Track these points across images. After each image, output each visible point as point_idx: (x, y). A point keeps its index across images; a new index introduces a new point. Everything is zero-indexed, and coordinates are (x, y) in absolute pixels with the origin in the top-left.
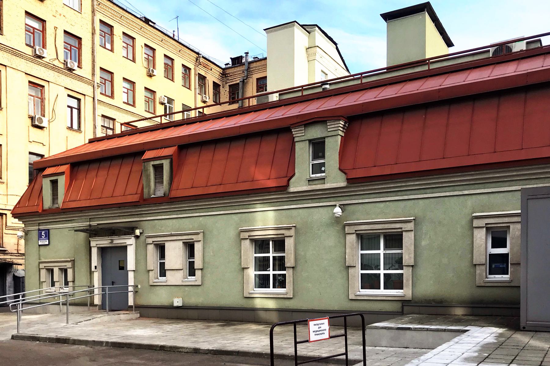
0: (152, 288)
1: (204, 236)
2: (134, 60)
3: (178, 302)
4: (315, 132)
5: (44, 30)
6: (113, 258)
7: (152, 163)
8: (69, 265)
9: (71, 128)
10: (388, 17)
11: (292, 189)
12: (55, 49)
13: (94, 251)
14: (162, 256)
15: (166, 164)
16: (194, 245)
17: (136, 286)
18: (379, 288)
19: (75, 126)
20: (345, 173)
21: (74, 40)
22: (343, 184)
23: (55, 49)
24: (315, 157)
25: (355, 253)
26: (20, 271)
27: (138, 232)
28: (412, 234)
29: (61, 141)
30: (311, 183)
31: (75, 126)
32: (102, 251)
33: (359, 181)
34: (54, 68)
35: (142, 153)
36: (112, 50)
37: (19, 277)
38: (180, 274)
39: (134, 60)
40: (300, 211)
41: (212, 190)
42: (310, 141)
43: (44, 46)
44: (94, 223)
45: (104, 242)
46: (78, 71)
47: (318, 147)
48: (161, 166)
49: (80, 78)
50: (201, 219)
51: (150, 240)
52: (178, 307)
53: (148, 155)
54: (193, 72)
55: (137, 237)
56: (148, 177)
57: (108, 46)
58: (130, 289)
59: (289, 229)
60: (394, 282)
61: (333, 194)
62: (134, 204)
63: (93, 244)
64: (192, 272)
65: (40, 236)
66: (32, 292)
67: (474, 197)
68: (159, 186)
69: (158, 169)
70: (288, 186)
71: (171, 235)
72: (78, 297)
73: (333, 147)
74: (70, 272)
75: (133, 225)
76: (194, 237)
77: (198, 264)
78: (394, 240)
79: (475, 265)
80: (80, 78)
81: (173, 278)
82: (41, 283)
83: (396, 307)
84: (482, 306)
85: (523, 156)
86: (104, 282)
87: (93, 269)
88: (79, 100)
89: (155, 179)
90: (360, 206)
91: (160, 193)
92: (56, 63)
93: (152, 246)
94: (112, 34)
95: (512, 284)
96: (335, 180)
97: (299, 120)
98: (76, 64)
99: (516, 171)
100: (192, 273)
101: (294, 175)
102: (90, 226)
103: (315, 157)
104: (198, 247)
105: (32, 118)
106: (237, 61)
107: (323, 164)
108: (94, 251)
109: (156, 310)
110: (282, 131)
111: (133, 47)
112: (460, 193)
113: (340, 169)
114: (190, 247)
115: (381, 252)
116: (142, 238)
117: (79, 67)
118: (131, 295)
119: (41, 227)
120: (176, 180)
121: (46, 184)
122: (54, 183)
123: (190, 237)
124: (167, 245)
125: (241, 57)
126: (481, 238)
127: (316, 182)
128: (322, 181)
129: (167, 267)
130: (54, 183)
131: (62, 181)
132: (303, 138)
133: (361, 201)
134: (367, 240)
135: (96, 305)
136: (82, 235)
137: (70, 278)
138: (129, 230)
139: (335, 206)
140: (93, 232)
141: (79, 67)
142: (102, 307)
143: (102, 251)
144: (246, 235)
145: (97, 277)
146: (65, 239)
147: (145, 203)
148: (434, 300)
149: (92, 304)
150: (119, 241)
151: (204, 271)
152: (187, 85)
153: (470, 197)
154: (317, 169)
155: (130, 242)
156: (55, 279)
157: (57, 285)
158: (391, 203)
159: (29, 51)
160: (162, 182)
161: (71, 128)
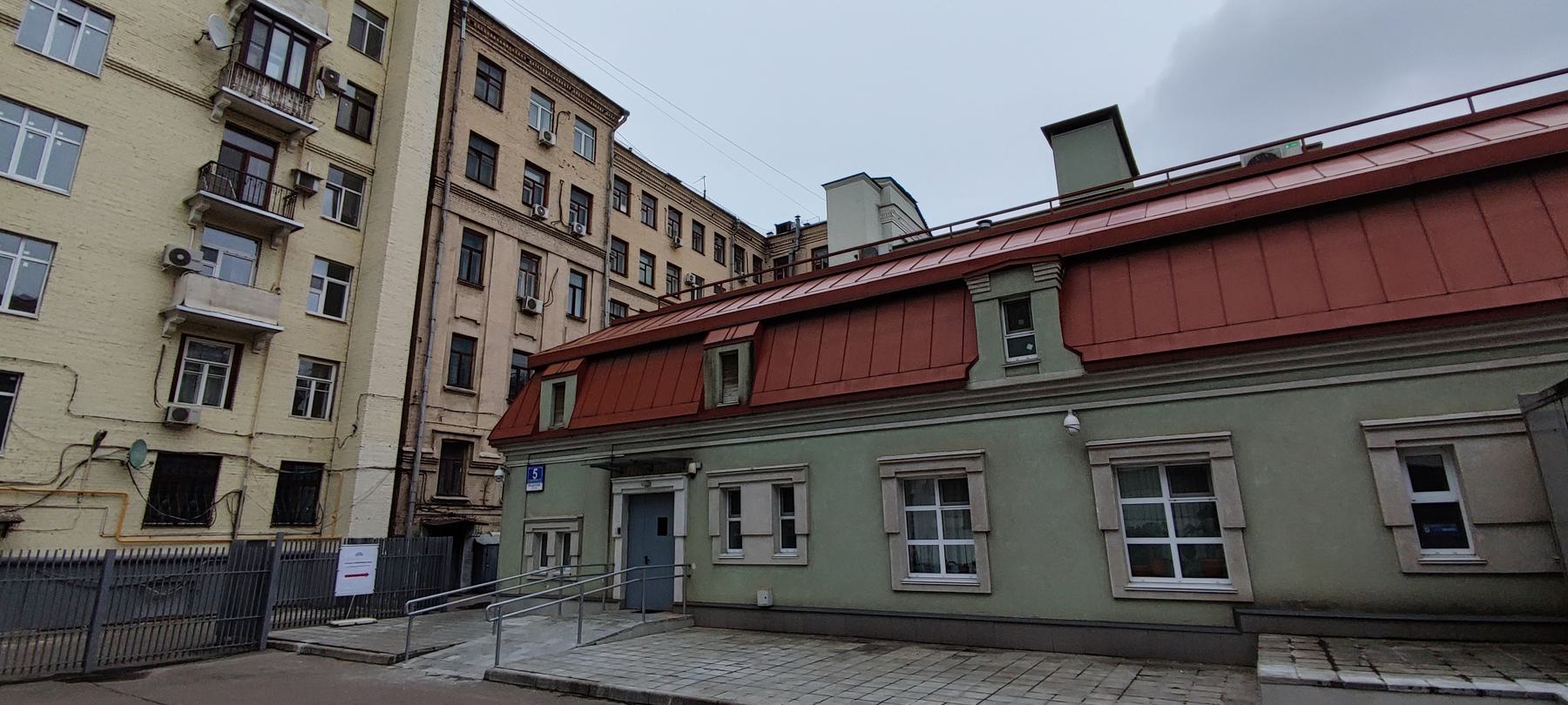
0: (718, 569)
1: (809, 474)
2: (655, 228)
3: (763, 599)
4: (1012, 285)
5: (546, 185)
6: (651, 514)
7: (720, 350)
8: (574, 526)
9: (571, 316)
10: (1051, 132)
11: (974, 385)
12: (556, 210)
13: (618, 502)
14: (735, 508)
15: (743, 351)
16: (1209, 466)
17: (687, 566)
18: (1173, 576)
19: (577, 314)
20: (1080, 354)
21: (582, 198)
22: (1078, 371)
23: (556, 210)
24: (1012, 327)
25: (1111, 504)
26: (487, 537)
27: (692, 467)
28: (981, 477)
29: (555, 332)
30: (1010, 372)
31: (577, 314)
32: (631, 500)
33: (1107, 370)
34: (556, 234)
35: (704, 335)
36: (628, 214)
37: (483, 546)
38: (768, 544)
39: (655, 228)
40: (992, 424)
41: (823, 391)
42: (1000, 299)
43: (545, 205)
44: (619, 453)
45: (634, 485)
46: (586, 239)
47: (1018, 311)
48: (735, 354)
49: (588, 248)
50: (803, 442)
51: (715, 482)
52: (765, 608)
53: (712, 338)
54: (728, 243)
55: (692, 476)
56: (712, 373)
57: (623, 209)
58: (678, 571)
59: (973, 458)
60: (1209, 563)
61: (1056, 392)
62: (690, 420)
63: (616, 489)
64: (789, 540)
65: (530, 476)
66: (507, 577)
67: (1352, 389)
68: (730, 389)
69: (730, 360)
70: (967, 378)
71: (753, 472)
72: (592, 585)
73: (1045, 308)
74: (574, 539)
75: (686, 455)
76: (970, 466)
77: (800, 527)
78: (955, 489)
79: (1390, 528)
80: (588, 248)
81: (759, 550)
82: (524, 558)
83: (1223, 616)
84: (1427, 617)
85: (1505, 298)
86: (629, 559)
87: (614, 534)
88: (584, 277)
89: (724, 376)
90: (1112, 413)
91: (731, 399)
92: (559, 227)
93: (717, 492)
94: (629, 194)
95: (1487, 570)
96: (1063, 367)
97: (972, 268)
98: (584, 228)
99: (1425, 338)
100: (789, 540)
101: (977, 359)
102: (612, 457)
103: (1012, 327)
104: (800, 493)
105: (520, 301)
106: (783, 228)
107: (1031, 339)
108: (618, 502)
109: (724, 612)
110: (951, 285)
111: (655, 210)
112: (1321, 382)
113: (1066, 346)
114: (785, 496)
115: (1166, 499)
116: (700, 478)
117: (588, 233)
118: (678, 582)
119: (532, 462)
120: (761, 372)
121: (547, 389)
122: (559, 389)
123: (785, 475)
124: (744, 490)
125: (789, 223)
126: (1391, 473)
127: (1021, 371)
128: (1034, 369)
129: (744, 531)
130: (559, 389)
131: (571, 383)
132: (988, 296)
133: (1111, 403)
134: (1132, 478)
135: (616, 601)
136: (600, 472)
137: (574, 551)
138: (678, 465)
139: (1066, 412)
140: (617, 469)
141: (588, 233)
142: (624, 604)
143: (631, 500)
144: (891, 471)
145: (619, 546)
146: (571, 483)
147: (704, 415)
148: (1306, 604)
149: (610, 600)
150: (659, 483)
151: (813, 537)
152: (719, 258)
153: (1344, 389)
154: (1017, 348)
155: (678, 483)
156: (550, 551)
157: (551, 562)
158: (1174, 406)
159: (524, 210)
160: (736, 381)
161: (571, 316)
